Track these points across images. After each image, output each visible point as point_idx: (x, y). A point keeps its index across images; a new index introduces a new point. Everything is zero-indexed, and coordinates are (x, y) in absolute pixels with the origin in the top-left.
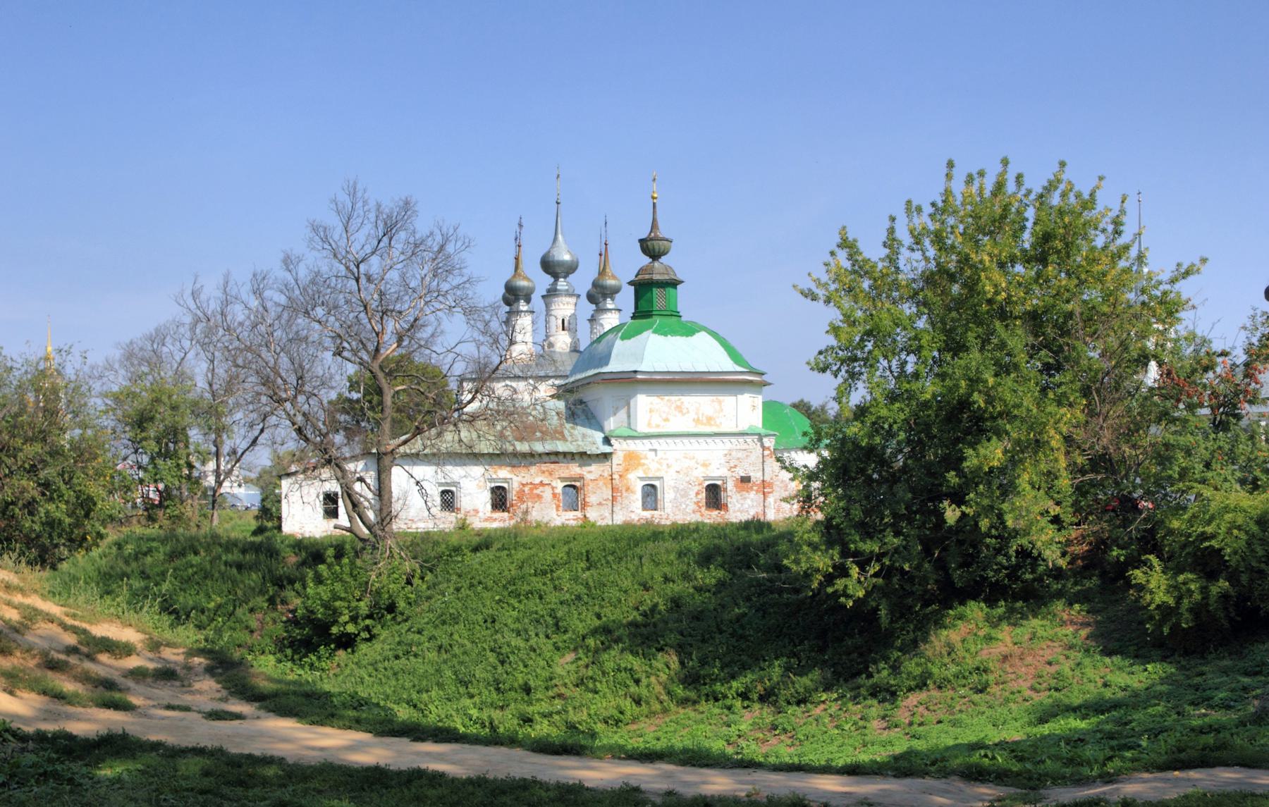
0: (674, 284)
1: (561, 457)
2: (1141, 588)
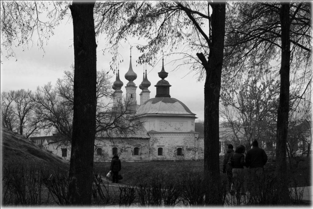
0: (171, 86)
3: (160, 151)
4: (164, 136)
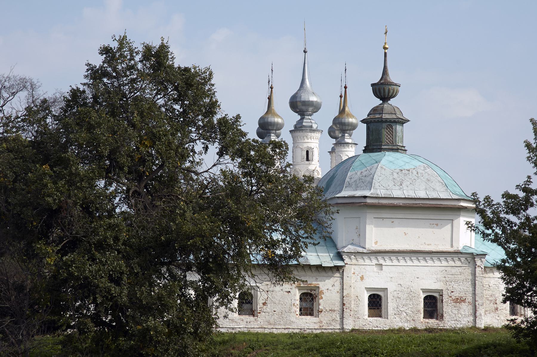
0: (402, 122)
3: (376, 303)
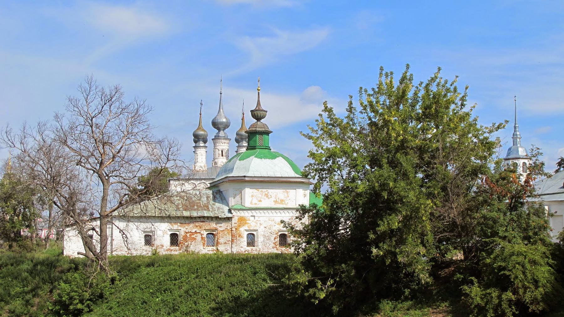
0: (267, 133)
1: (206, 219)
2: (467, 295)
4: (257, 213)
